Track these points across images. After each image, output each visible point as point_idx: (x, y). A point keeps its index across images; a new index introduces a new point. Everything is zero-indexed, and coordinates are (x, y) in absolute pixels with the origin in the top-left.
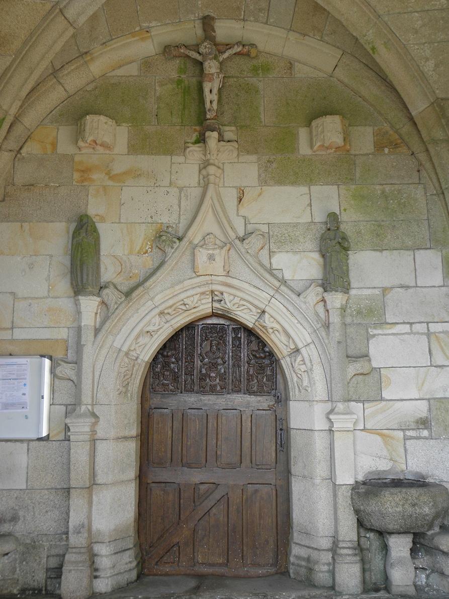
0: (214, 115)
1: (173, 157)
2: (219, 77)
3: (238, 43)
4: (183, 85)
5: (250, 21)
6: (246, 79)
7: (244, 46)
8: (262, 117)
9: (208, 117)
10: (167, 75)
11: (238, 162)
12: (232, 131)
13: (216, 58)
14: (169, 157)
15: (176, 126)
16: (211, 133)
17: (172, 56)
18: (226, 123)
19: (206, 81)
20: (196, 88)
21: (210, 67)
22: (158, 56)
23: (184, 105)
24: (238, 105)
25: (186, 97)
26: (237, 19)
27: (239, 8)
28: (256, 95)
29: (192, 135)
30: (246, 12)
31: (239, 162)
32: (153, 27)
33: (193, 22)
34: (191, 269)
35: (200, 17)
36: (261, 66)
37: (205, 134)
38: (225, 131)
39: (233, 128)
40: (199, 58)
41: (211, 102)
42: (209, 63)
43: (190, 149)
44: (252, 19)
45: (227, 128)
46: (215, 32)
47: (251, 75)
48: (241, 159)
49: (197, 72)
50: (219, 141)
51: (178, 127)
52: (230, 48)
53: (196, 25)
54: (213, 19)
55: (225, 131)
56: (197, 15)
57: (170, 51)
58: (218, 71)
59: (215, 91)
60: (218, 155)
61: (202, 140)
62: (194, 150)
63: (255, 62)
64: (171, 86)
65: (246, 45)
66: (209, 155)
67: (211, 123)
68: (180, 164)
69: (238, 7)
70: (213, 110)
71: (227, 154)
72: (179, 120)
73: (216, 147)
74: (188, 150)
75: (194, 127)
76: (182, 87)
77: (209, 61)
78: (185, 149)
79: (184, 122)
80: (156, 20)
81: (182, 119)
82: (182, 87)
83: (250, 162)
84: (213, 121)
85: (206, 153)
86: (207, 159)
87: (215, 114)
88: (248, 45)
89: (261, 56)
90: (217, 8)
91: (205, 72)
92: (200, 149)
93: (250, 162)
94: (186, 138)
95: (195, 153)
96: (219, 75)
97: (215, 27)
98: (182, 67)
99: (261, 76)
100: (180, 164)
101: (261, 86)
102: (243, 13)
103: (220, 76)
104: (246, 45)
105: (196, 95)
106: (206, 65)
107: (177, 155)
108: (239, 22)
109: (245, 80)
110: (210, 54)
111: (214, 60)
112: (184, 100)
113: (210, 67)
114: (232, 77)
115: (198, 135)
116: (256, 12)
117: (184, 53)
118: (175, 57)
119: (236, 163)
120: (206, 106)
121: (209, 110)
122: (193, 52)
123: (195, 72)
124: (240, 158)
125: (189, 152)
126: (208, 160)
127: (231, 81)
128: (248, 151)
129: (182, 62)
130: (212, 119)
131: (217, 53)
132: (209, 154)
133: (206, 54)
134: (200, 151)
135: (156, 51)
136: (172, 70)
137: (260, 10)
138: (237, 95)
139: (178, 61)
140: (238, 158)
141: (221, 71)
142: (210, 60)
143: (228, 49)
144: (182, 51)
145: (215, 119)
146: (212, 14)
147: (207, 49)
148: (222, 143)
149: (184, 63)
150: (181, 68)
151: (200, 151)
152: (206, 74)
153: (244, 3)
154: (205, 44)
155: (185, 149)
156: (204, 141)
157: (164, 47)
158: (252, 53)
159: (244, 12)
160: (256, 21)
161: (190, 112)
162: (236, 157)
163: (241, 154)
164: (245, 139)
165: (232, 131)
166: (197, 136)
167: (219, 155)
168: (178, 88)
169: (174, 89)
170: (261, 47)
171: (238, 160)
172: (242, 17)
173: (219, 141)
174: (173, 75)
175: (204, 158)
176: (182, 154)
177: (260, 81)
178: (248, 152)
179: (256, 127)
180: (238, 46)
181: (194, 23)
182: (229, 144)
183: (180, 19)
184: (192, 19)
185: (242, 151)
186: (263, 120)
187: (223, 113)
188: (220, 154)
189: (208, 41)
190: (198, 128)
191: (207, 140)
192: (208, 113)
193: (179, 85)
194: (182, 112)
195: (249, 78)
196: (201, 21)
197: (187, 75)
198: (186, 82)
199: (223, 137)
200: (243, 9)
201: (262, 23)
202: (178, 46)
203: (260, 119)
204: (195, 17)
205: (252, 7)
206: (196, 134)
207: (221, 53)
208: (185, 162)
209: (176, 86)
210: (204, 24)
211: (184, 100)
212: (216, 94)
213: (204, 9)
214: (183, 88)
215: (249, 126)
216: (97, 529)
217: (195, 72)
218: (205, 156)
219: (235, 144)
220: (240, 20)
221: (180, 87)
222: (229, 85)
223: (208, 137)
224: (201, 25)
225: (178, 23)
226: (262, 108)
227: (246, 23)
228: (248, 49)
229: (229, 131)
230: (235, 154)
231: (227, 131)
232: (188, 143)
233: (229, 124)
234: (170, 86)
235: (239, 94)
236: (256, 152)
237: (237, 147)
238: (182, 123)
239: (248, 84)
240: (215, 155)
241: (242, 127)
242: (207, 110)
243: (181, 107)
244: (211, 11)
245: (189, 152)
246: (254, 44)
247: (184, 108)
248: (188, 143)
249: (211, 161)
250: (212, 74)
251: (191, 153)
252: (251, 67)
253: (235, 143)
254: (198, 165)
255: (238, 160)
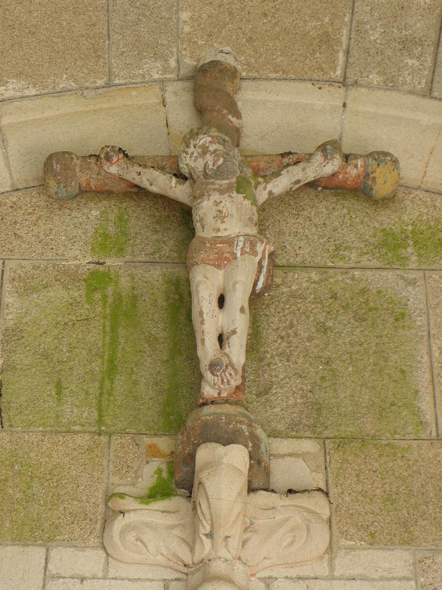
0: (234, 384)
1: (53, 553)
2: (255, 254)
3: (328, 148)
4: (110, 290)
5: (369, 86)
6: (357, 273)
7: (347, 158)
8: (425, 404)
9: (208, 391)
10: (50, 255)
11: (331, 578)
12: (303, 456)
13: (241, 186)
14: (37, 554)
15: (75, 432)
16: (220, 449)
17: (73, 189)
18: (281, 427)
19: (203, 261)
20: (161, 302)
21: (221, 216)
22: (19, 193)
23: (111, 361)
24: (327, 363)
25: (122, 332)
26: (321, 81)
27: (327, 40)
28: (396, 329)
29: (139, 468)
30: (355, 52)
31: (336, 574)
32: (11, 100)
33: (157, 89)
34: (315, 576)
35: (183, 72)
36: (413, 232)
37: (192, 457)
38: (275, 456)
39: (309, 446)
40: (179, 191)
41: (221, 339)
42: (217, 204)
43: (129, 518)
44: (375, 78)
45: (282, 446)
46: (238, 115)
47: (375, 263)
48: (344, 564)
49: (168, 248)
50: (251, 490)
51: (83, 440)
52: (296, 163)
53: (170, 98)
54: (233, 73)
55: (275, 456)
56: (173, 63)
57: (66, 167)
58: (253, 231)
59: (239, 297)
60: (244, 543)
61: (179, 485)
62: (147, 525)
63: (387, 219)
64: (62, 293)
65: (356, 157)
66: (207, 541)
67: (219, 415)
68: (82, 579)
69: (326, 33)
70: (231, 364)
71: (285, 543)
72: (89, 414)
73: (238, 507)
74: (119, 523)
75: (147, 440)
76: (105, 297)
77: (216, 197)
78: (110, 515)
79: (108, 420)
80: (19, 75)
81: (100, 410)
82: (105, 297)
83: (382, 579)
84: (228, 409)
85: (195, 532)
86: (197, 559)
87: (236, 382)
88: (361, 156)
89: (412, 201)
90: (250, 40)
91: (199, 233)
92: (171, 520)
93: (382, 579)
94: (115, 479)
95: (149, 536)
96: (253, 245)
97: (240, 104)
98: (111, 229)
99: (414, 266)
100: (82, 579)
101: (414, 297)
102: (341, 56)
103: (260, 248)
104: (356, 157)
105: (161, 326)
106: (205, 209)
107: (70, 543)
108: (326, 88)
109: (353, 279)
110: (219, 173)
111: (235, 194)
112: (114, 340)
113: (221, 216)
114: (305, 267)
115: (164, 467)
116: (389, 53)
117: (121, 179)
118: (85, 193)
119: (325, 579)
120: (200, 353)
121: (214, 366)
122: (156, 173)
123: (159, 250)
124: (337, 562)
125: (123, 532)
126: (204, 563)
127: (300, 281)
128: (372, 535)
129: (112, 217)
130: (226, 401)
131: (249, 172)
132: (210, 535)
133: (206, 175)
134: (173, 527)
135: (16, 176)
136: (73, 240)
137: (406, 45)
138: (323, 329)
139: (95, 213)
140: (331, 560)
141: (261, 232)
142: (222, 192)
143: (288, 165)
144: (114, 170)
145: (238, 403)
146: (230, 60)
147: (209, 158)
148: (262, 497)
149: (120, 218)
150: (106, 236)
151: (173, 527)
152: (203, 241)
153: (347, 19)
154: (204, 140)
155: (106, 522)
156: (190, 488)
157: (43, 160)
158: (379, 181)
159: (347, 52)
160: (391, 84)
161: (136, 383)
162: (321, 558)
163: (344, 542)
164: (359, 488)
165: (303, 456)
166: (159, 471)
167: (249, 545)
168: (89, 300)
169: (74, 304)
170: (410, 171)
171: (332, 567)
172: (339, 72)
173: (251, 490)
174: (76, 258)
175: (187, 558)
176: (93, 541)
177: (413, 283)
178: (373, 540)
179: (404, 444)
180: (326, 157)
181: (163, 90)
182: (296, 500)
183: (110, 74)
184: (156, 76)
185: (345, 534)
186: (429, 417)
187: (267, 391)
188: (255, 540)
189: (214, 132)
190: (164, 443)
191: (203, 476)
192: (208, 375)
193: (95, 290)
194: (102, 382)
195: (369, 272)
196: (188, 84)
197: (128, 257)
198: (125, 283)
199: (267, 472)
200: (344, 39)
201: (411, 92)
202: (97, 157)
203: (417, 412)
204: (165, 70)
205: (374, 36)
206: (157, 464)
207: (264, 177)
208: (106, 570)
209: (83, 292)
210: (197, 90)
211: (114, 340)
212: (242, 310)
213: (201, 42)
214: (110, 300)
215: (374, 437)
216: (360, 290)
217: (159, 250)
218: (192, 550)
219: (319, 505)
220: (331, 82)
221: (98, 296)
222: (293, 295)
223: (207, 465)
224: (187, 97)
225: (101, 91)
226: (422, 378)
227: (354, 93)
228: (365, 166)
229: (290, 455)
230: (321, 540)
231: (283, 456)
232: (122, 496)
233: (294, 431)
234: (58, 294)
235: (329, 324)
236: (408, 542)
237: (326, 513)
238: (100, 421)
239: (364, 291)
240: (234, 543)
241: (342, 442)
242: (204, 364)
243: (97, 366)
244: (228, 49)
245: (123, 532)
246: (386, 154)
247: (112, 370)
248: (122, 496)
249: (218, 567)
250: (230, 241)
251: (131, 537)
252: (374, 236)
253: (320, 498)
254: (162, 584)
255: (332, 567)
